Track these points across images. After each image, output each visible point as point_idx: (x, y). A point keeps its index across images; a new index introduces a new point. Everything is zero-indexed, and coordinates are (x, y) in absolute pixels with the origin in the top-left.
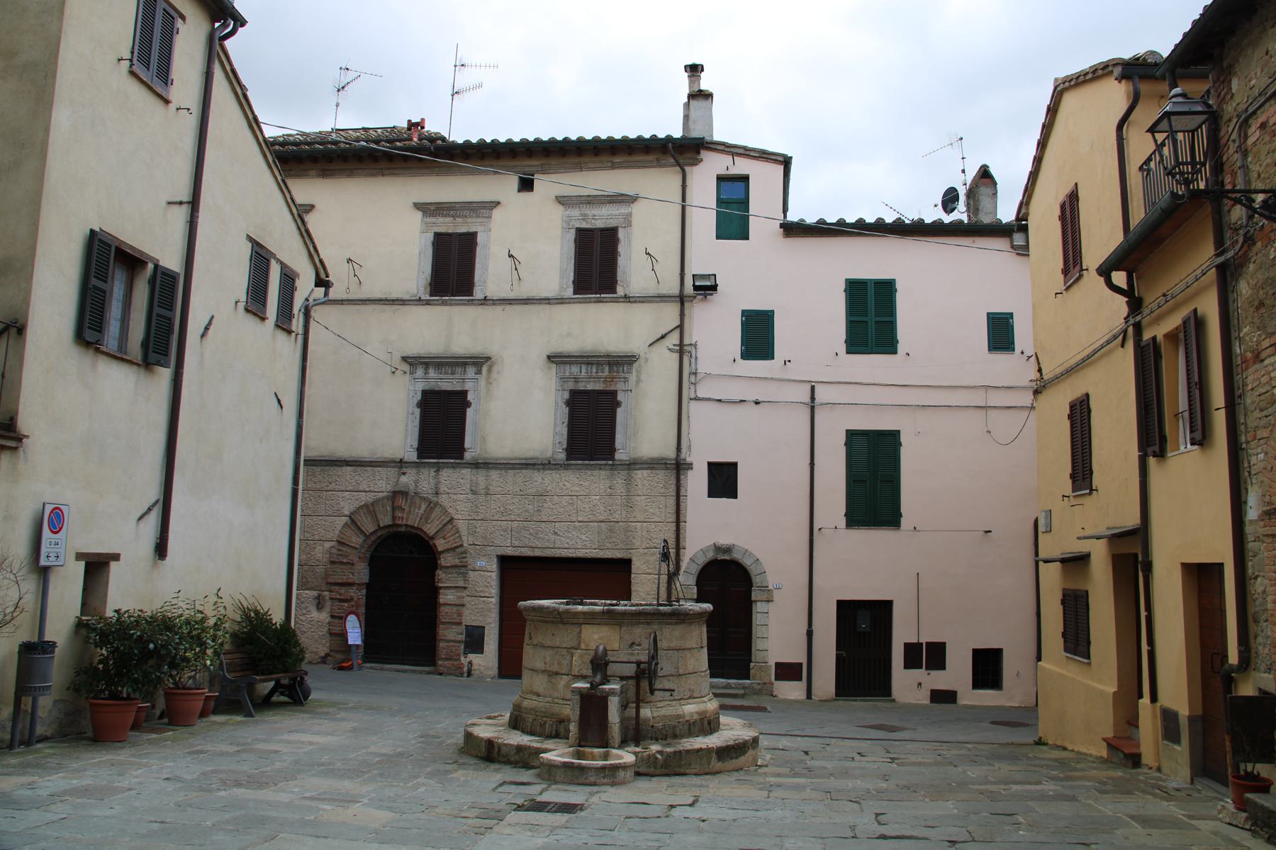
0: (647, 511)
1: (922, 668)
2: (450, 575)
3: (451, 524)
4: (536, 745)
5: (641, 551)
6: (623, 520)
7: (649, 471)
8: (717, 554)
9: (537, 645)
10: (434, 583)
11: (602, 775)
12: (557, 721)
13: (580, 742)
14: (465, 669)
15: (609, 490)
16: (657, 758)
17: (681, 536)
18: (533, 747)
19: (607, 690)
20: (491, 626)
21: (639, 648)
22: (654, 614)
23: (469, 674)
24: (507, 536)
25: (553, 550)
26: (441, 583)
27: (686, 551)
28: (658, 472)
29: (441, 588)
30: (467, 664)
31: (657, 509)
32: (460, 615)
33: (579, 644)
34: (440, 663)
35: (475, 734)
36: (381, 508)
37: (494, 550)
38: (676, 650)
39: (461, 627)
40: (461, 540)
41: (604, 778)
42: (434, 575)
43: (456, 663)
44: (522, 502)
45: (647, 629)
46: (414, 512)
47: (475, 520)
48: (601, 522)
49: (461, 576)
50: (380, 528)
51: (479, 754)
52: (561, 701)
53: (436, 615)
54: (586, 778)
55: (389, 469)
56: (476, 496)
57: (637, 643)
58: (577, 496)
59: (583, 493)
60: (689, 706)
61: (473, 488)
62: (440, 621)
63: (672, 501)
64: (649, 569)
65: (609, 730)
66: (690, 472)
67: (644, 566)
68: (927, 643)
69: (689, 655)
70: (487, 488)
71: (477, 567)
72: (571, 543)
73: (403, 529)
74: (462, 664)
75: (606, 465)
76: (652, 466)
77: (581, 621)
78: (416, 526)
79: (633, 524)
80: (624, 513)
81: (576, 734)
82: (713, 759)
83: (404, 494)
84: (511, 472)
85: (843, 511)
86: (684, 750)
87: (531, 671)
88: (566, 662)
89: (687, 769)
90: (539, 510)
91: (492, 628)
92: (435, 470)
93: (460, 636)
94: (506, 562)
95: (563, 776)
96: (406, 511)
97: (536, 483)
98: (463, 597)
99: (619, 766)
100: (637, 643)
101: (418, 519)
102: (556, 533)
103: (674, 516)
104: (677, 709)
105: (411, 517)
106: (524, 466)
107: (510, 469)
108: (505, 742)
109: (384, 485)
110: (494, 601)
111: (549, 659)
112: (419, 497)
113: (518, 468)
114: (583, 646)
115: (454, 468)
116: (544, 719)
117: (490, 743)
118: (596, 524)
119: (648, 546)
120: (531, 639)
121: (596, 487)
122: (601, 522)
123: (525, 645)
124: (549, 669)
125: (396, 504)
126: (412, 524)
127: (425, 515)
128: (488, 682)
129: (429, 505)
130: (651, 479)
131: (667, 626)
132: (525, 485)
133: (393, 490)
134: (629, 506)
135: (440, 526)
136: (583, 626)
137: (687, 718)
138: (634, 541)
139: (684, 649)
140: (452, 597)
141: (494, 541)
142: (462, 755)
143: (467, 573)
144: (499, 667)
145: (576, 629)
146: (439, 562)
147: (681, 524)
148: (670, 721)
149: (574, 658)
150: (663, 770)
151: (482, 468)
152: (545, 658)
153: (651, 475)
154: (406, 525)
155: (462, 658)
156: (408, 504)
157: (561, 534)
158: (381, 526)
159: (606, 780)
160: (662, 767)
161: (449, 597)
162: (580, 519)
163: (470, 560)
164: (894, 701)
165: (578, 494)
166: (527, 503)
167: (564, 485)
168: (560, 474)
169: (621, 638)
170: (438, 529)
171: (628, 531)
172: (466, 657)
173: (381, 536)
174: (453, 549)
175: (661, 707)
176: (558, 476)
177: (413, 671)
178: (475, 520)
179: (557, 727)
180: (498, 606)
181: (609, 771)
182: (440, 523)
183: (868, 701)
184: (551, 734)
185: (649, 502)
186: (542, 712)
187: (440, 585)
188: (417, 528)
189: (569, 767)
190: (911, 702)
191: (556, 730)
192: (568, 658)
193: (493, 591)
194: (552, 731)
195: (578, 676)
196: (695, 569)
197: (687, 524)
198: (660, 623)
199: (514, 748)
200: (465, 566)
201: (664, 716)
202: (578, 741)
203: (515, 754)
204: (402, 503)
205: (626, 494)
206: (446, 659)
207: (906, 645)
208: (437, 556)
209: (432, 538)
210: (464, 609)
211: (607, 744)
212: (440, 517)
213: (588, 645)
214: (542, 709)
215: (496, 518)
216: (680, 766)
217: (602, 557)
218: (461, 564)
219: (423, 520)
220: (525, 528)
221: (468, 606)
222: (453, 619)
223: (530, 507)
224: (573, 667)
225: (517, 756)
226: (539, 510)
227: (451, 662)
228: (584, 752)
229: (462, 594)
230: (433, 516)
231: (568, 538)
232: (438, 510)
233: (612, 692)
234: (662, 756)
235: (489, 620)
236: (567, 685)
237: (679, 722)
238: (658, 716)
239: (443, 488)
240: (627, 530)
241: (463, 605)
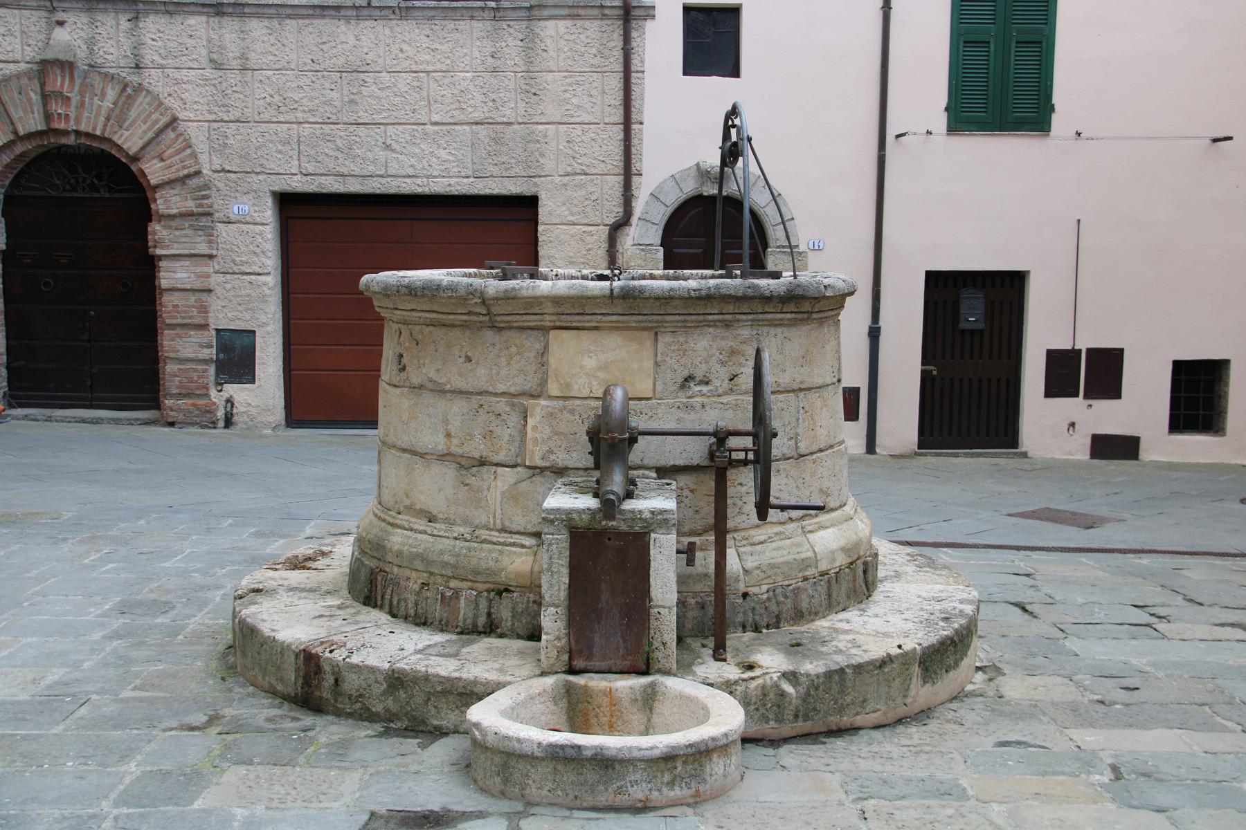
0: (566, 101)
1: (1077, 395)
2: (177, 233)
3: (174, 130)
4: (445, 668)
5: (557, 180)
6: (521, 121)
7: (569, 23)
8: (703, 184)
9: (421, 387)
10: (148, 248)
11: (667, 778)
12: (488, 591)
13: (570, 658)
14: (221, 413)
15: (490, 60)
16: (783, 694)
17: (633, 150)
18: (437, 675)
19: (647, 515)
20: (269, 328)
21: (705, 389)
22: (745, 298)
23: (229, 422)
24: (291, 153)
25: (383, 181)
26: (162, 248)
27: (643, 179)
28: (587, 23)
29: (160, 258)
30: (224, 403)
31: (586, 99)
32: (204, 309)
33: (543, 383)
34: (168, 402)
35: (265, 628)
36: (16, 95)
37: (265, 181)
38: (793, 391)
39: (206, 333)
40: (197, 162)
41: (671, 784)
42: (146, 233)
43: (201, 402)
44: (316, 86)
45: (723, 338)
46: (92, 105)
47: (222, 121)
48: (477, 123)
49: (201, 233)
50: (19, 138)
51: (280, 688)
52: (495, 536)
53: (155, 312)
54: (619, 791)
55: (27, 13)
56: (221, 73)
57: (699, 375)
58: (428, 72)
59: (438, 66)
60: (822, 533)
61: (215, 56)
62: (164, 322)
63: (616, 82)
64: (572, 214)
65: (653, 623)
66: (649, 24)
67: (564, 208)
68: (1089, 350)
69: (819, 403)
70: (243, 57)
71: (231, 216)
72: (419, 166)
73: (71, 140)
74: (214, 403)
75: (483, 9)
76: (575, 11)
77: (548, 320)
78: (98, 133)
79: (540, 127)
80: (521, 105)
81: (558, 638)
82: (914, 680)
83: (67, 66)
84: (291, 24)
85: (943, 101)
86: (848, 666)
87: (407, 455)
88: (506, 433)
89: (857, 714)
90: (352, 101)
91: (268, 333)
92: (128, 16)
93: (207, 351)
94: (289, 203)
95: (550, 785)
96: (74, 102)
97: (345, 46)
98: (208, 276)
99: (711, 745)
100: (699, 375)
101: (102, 119)
102: (388, 147)
103: (621, 111)
104: (799, 545)
105: (86, 114)
106: (318, 11)
107: (289, 17)
108: (355, 659)
109: (18, 47)
110: (271, 281)
111: (457, 424)
112: (100, 73)
113: (303, 17)
114: (554, 389)
115: (170, 13)
116: (453, 584)
117: (310, 661)
118: (467, 128)
119: (569, 169)
120: (403, 369)
121: (466, 54)
122: (477, 123)
123: (383, 385)
124: (460, 451)
125: (49, 88)
126: (90, 131)
127: (117, 111)
128: (266, 436)
129: (124, 90)
130: (573, 37)
131: (773, 331)
132: (322, 50)
133: (38, 58)
134: (532, 93)
135: (150, 134)
136: (552, 333)
137: (823, 566)
138: (542, 161)
139: (809, 389)
140: (185, 275)
141: (265, 162)
142: (230, 682)
143: (213, 229)
144: (286, 407)
145: (532, 344)
146: (153, 206)
147: (634, 126)
148: (787, 578)
149: (530, 422)
150: (800, 723)
151: (231, 14)
152: (446, 422)
153: (574, 30)
154: (78, 133)
155: (213, 393)
156: (76, 88)
157: (398, 149)
158: (22, 132)
159: (677, 792)
160: (796, 716)
161: (178, 276)
162: (436, 118)
163: (217, 202)
164: (1024, 455)
165: (428, 69)
166: (327, 85)
167: (401, 50)
168: (391, 28)
169: (657, 364)
170: (146, 139)
171: (530, 142)
172: (221, 391)
173: (22, 155)
174: (183, 180)
175: (762, 543)
176: (387, 31)
177: (116, 421)
178: (222, 121)
179: (490, 607)
180: (278, 290)
181: (684, 763)
182: (150, 129)
183: (979, 455)
184: (475, 625)
185: (570, 85)
186: (445, 564)
187: (159, 252)
188: (102, 139)
189: (568, 760)
190: (1056, 457)
191: (489, 614)
192: (514, 419)
193: (269, 262)
194: (476, 617)
195: (543, 470)
196: (660, 215)
197: (644, 127)
198: (755, 323)
199: (380, 678)
200: (209, 214)
201: (772, 566)
202: (566, 657)
203: (384, 693)
204: (62, 86)
205: (524, 68)
206: (181, 396)
207: (1050, 353)
208: (149, 195)
209: (135, 159)
210: (213, 296)
211: (648, 664)
212: (149, 115)
213: (568, 386)
214: (446, 558)
215: (266, 117)
216: (841, 710)
217: (482, 193)
218: (200, 210)
219: (112, 121)
220: (327, 138)
221: (219, 291)
222: (191, 317)
223: (335, 95)
224: (529, 443)
225: (390, 702)
226: (352, 101)
227: (190, 401)
228: (585, 688)
229: (205, 269)
230: (133, 113)
231: (414, 155)
232: (142, 102)
233: (659, 520)
234: (794, 687)
235: (263, 318)
236: (513, 496)
237: (805, 579)
238: (758, 568)
239: (149, 56)
240: (528, 140)
241: (210, 291)
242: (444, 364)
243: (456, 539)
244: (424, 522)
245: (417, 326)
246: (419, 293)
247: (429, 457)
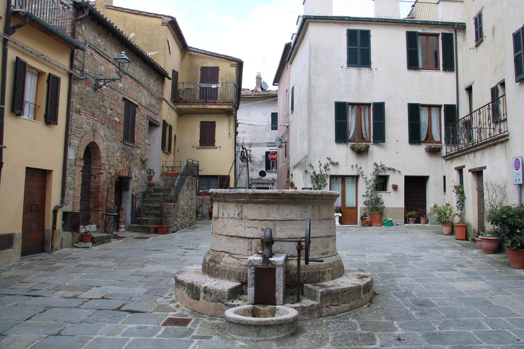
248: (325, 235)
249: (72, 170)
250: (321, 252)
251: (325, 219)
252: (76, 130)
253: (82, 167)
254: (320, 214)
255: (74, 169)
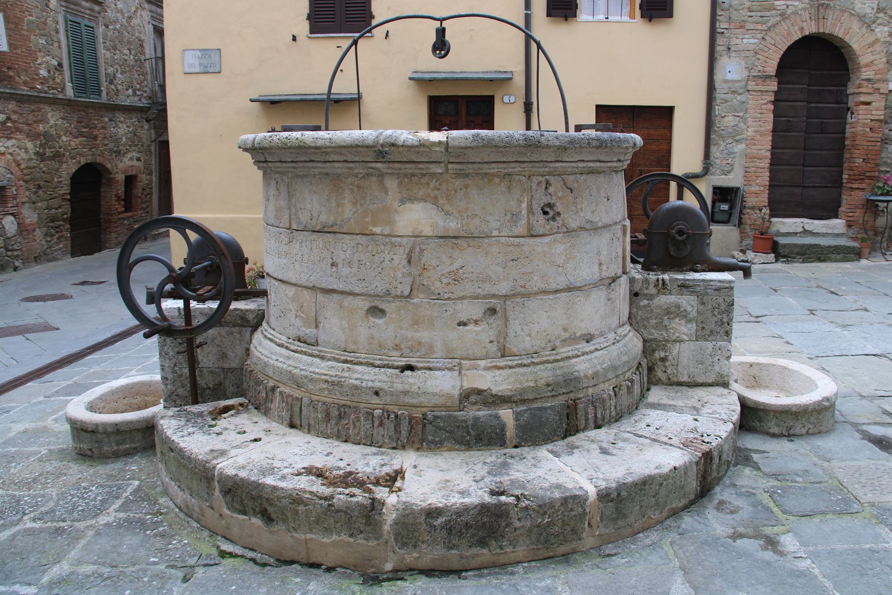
85: (306, 11)
152: (599, 253)
242: (597, 205)
243: (614, 343)
244: (584, 344)
245: (571, 176)
246: (609, 145)
247: (586, 288)
248: (303, 280)
249: (738, 103)
250: (293, 332)
251: (310, 228)
252: (751, 17)
253: (773, 94)
254: (293, 210)
255: (744, 99)
